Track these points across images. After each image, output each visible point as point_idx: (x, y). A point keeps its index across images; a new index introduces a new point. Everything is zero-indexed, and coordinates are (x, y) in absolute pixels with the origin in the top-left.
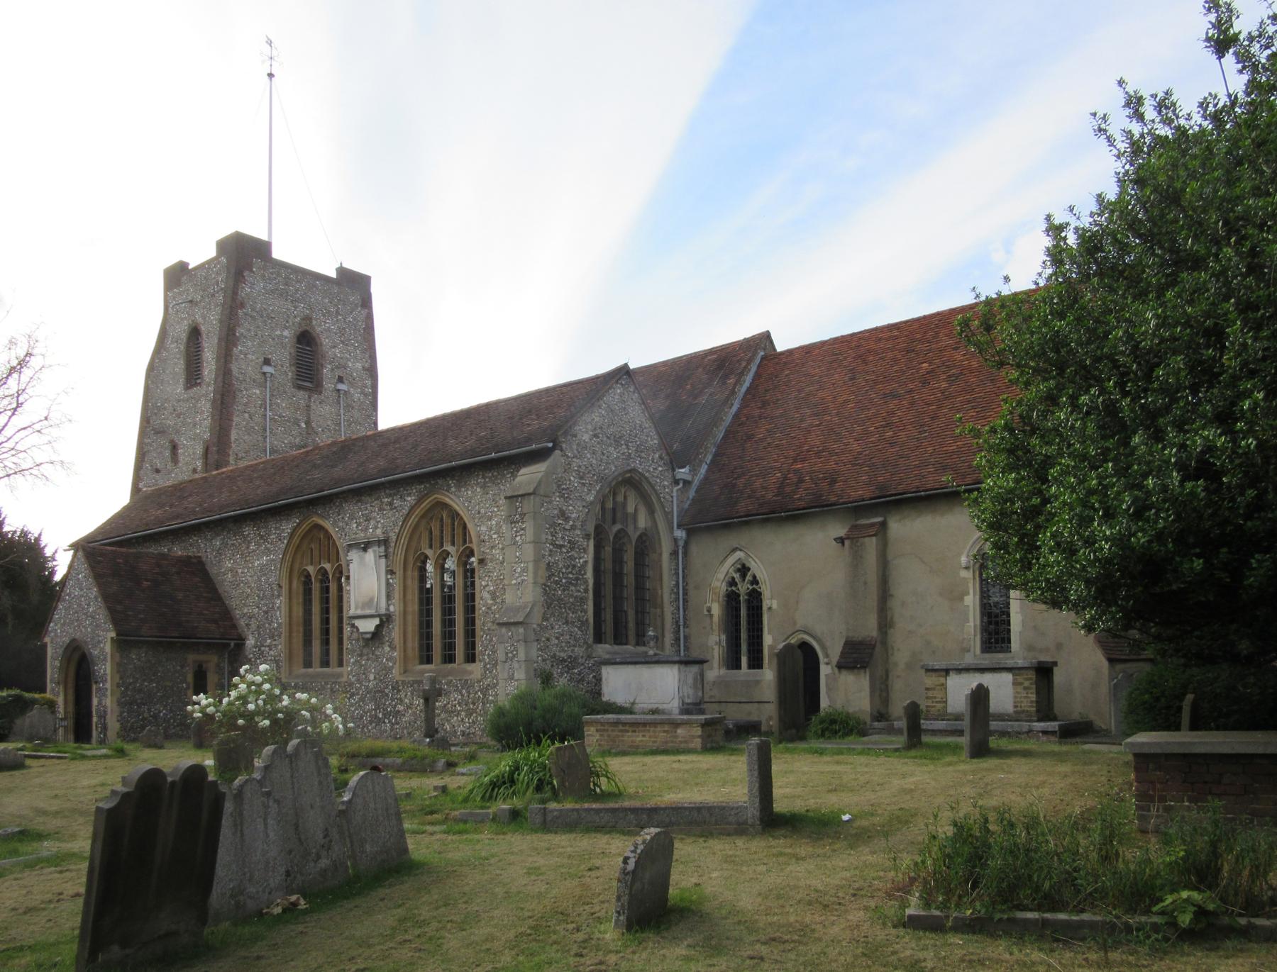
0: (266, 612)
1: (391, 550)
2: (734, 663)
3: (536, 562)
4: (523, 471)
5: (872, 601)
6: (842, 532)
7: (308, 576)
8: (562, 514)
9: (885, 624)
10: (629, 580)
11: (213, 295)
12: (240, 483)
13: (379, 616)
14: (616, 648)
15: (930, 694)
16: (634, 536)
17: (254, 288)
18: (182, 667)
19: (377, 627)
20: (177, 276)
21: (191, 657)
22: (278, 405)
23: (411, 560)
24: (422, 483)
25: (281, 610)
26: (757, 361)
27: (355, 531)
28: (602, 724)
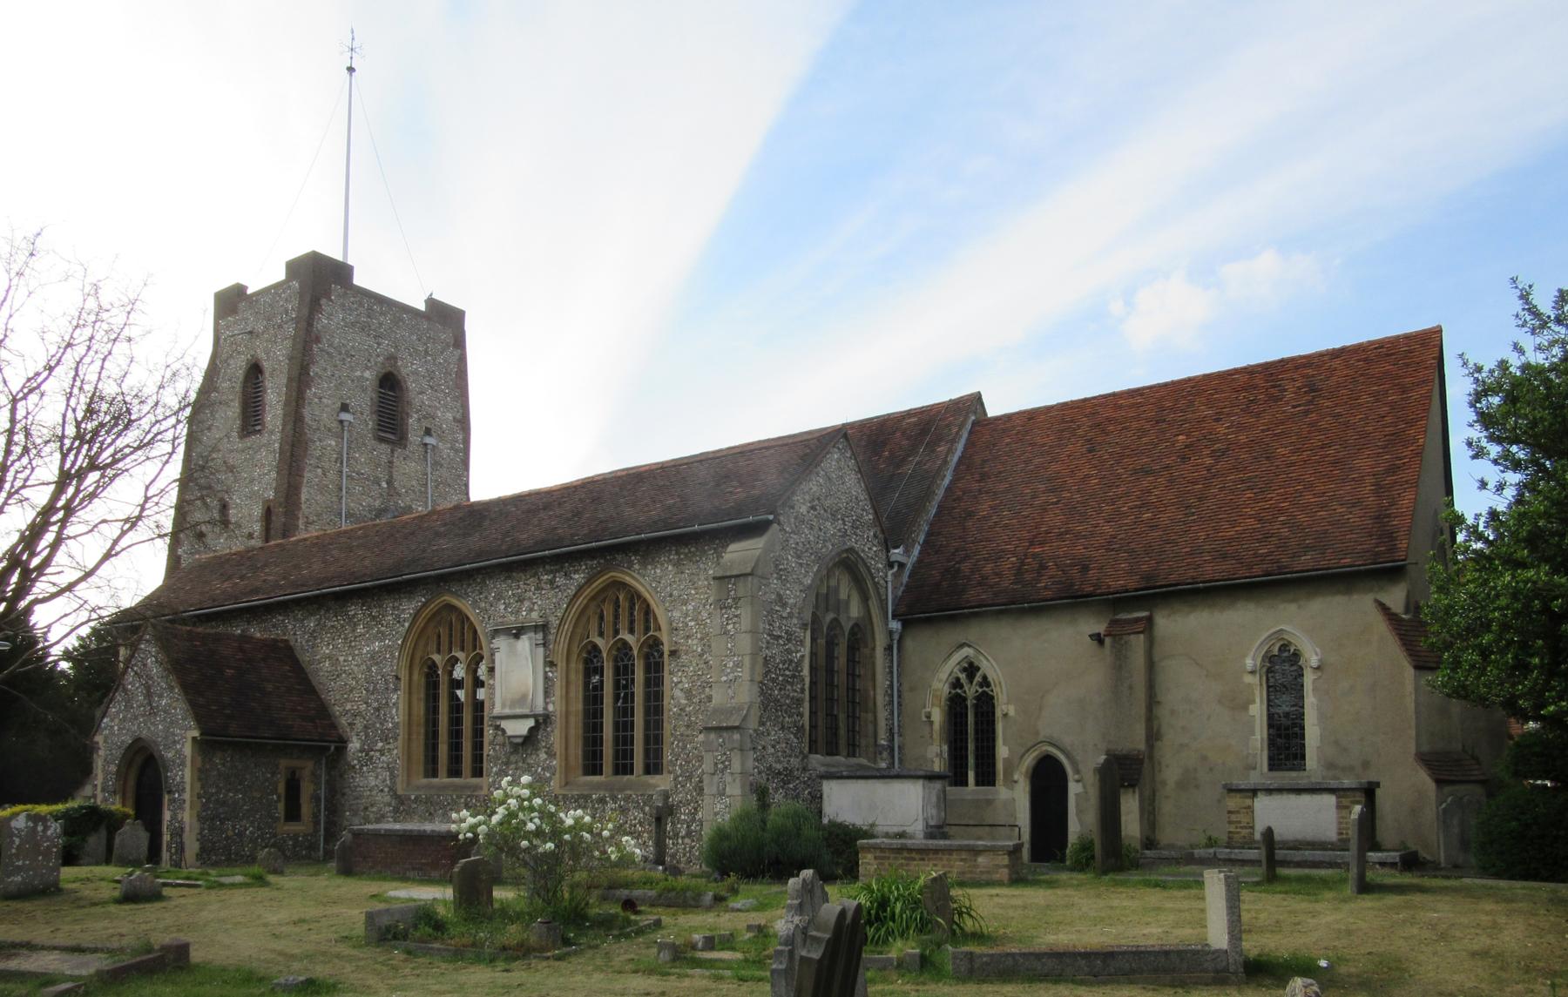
0: (377, 709)
1: (551, 637)
2: (432, 771)
3: (754, 655)
4: (732, 547)
5: (1140, 709)
6: (1100, 627)
7: (433, 666)
8: (781, 601)
9: (1153, 736)
10: (841, 679)
11: (280, 326)
12: (335, 553)
13: (535, 716)
14: (829, 759)
15: (1234, 817)
16: (847, 627)
17: (331, 319)
18: (273, 774)
19: (531, 729)
20: (231, 302)
21: (284, 763)
22: (356, 460)
23: (575, 650)
24: (593, 558)
25: (399, 708)
26: (968, 426)
27: (503, 613)
28: (882, 850)
